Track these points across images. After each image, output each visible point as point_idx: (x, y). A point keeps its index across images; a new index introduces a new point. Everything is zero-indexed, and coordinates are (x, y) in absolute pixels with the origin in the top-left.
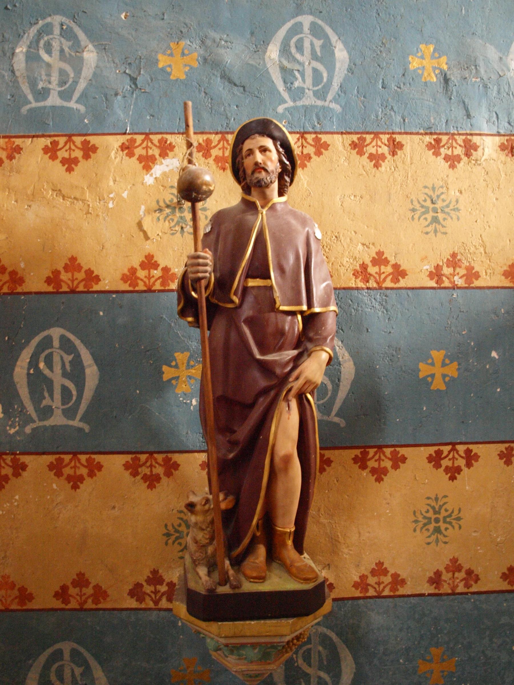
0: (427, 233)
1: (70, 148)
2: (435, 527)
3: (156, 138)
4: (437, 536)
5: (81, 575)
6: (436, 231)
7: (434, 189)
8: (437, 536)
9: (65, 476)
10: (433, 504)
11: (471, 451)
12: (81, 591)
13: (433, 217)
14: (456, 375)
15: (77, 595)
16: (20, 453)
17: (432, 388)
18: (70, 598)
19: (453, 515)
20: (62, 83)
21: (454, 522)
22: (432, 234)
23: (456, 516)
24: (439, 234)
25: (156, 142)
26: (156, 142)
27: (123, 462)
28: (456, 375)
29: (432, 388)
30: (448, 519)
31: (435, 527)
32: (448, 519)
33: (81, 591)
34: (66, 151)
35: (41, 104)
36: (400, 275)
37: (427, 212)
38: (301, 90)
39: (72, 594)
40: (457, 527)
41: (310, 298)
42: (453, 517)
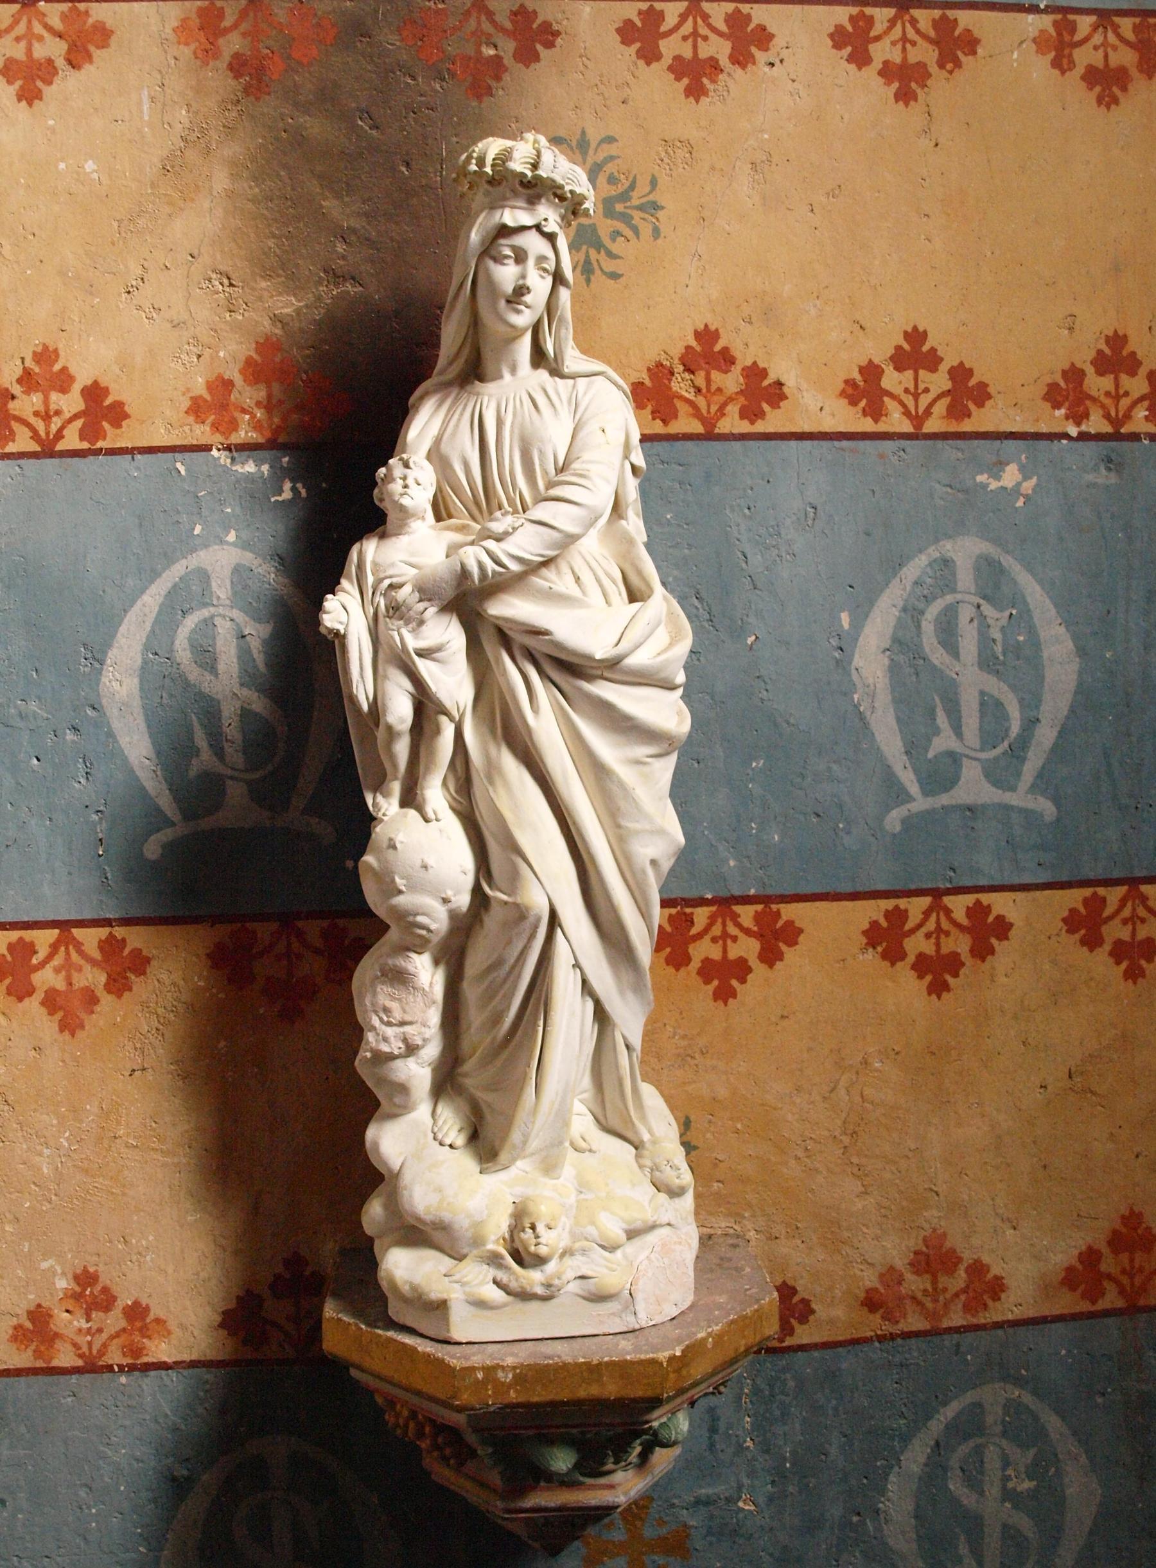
1: (916, 396)
3: (959, 905)
4: (587, 252)
5: (1108, 101)
8: (587, 252)
9: (911, 958)
11: (988, 909)
16: (1046, 6)
19: (634, 194)
20: (989, 739)
21: (637, 215)
23: (644, 200)
25: (960, 915)
26: (960, 915)
30: (619, 207)
32: (619, 207)
34: (894, 43)
35: (944, 799)
36: (849, 35)
40: (646, 230)
41: (552, 793)
42: (636, 202)
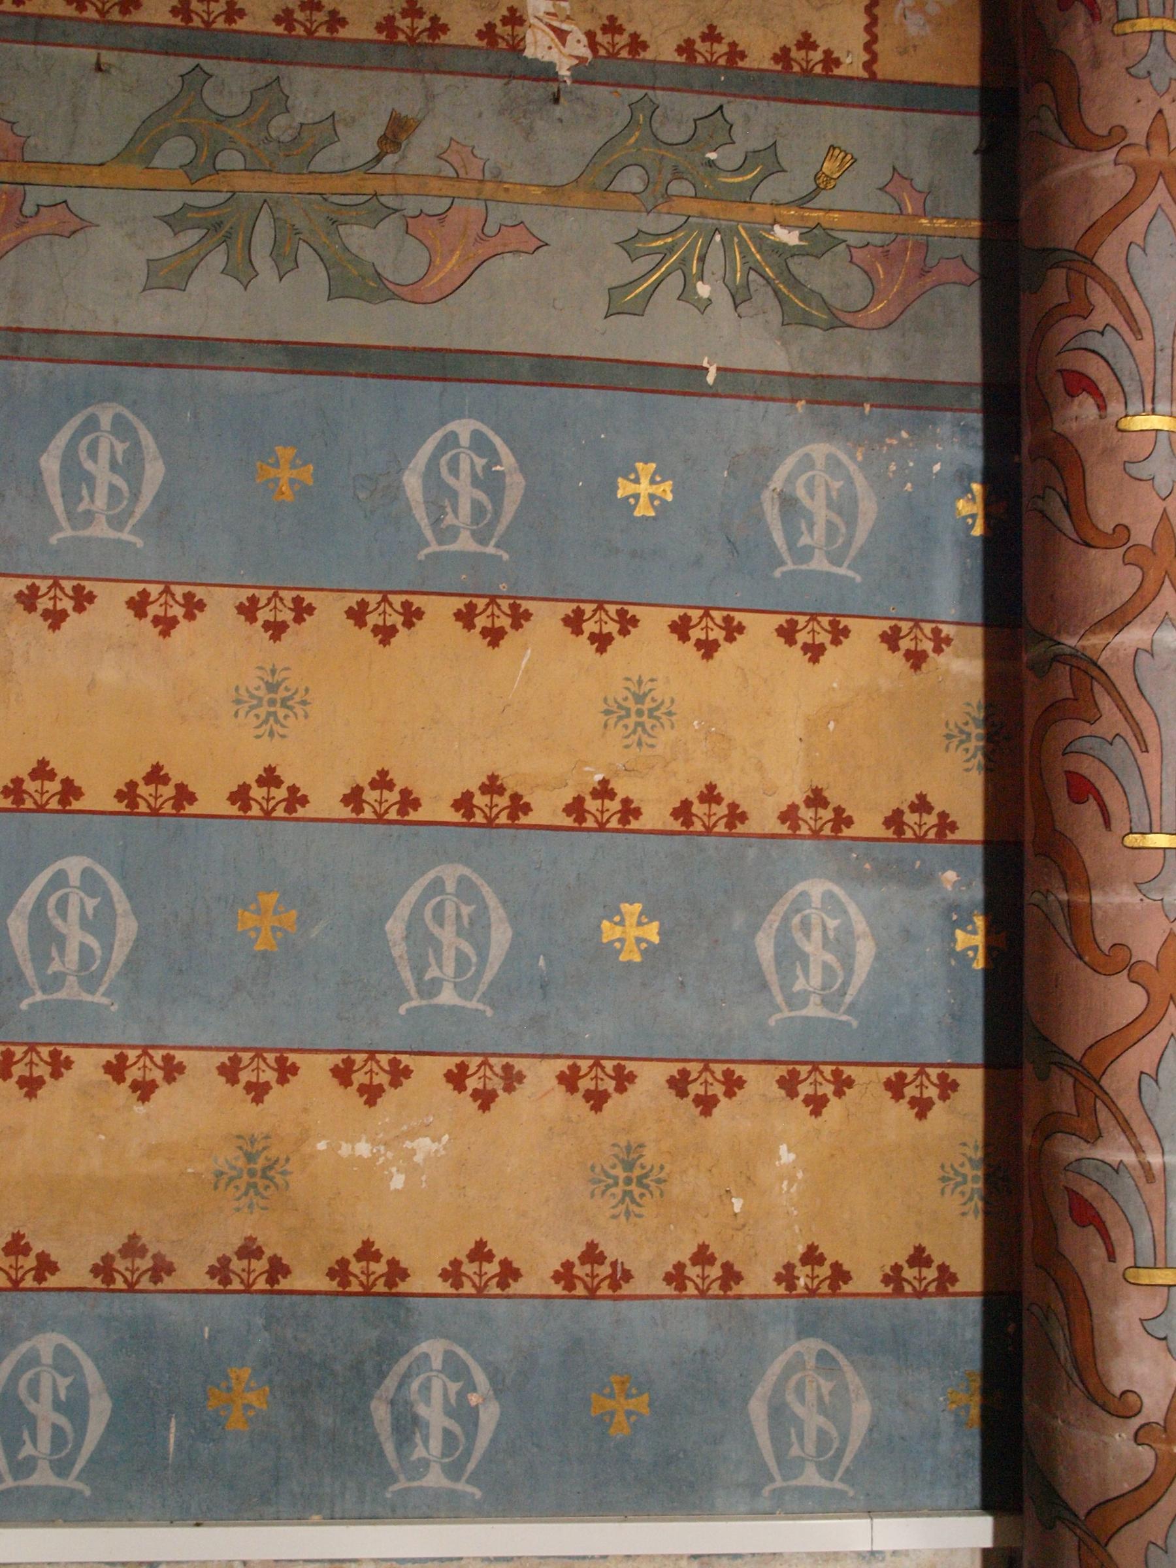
0: (652, 680)
2: (276, 693)
6: (640, 682)
7: (670, 714)
10: (277, 728)
12: (371, 1078)
13: (643, 703)
14: (621, 481)
15: (127, 1269)
17: (620, 480)
18: (49, 1060)
22: (645, 679)
24: (636, 678)
27: (958, 1284)
28: (621, 481)
29: (620, 480)
31: (276, 693)
33: (371, 1078)
37: (651, 711)
38: (425, 1464)
39: (289, 612)
